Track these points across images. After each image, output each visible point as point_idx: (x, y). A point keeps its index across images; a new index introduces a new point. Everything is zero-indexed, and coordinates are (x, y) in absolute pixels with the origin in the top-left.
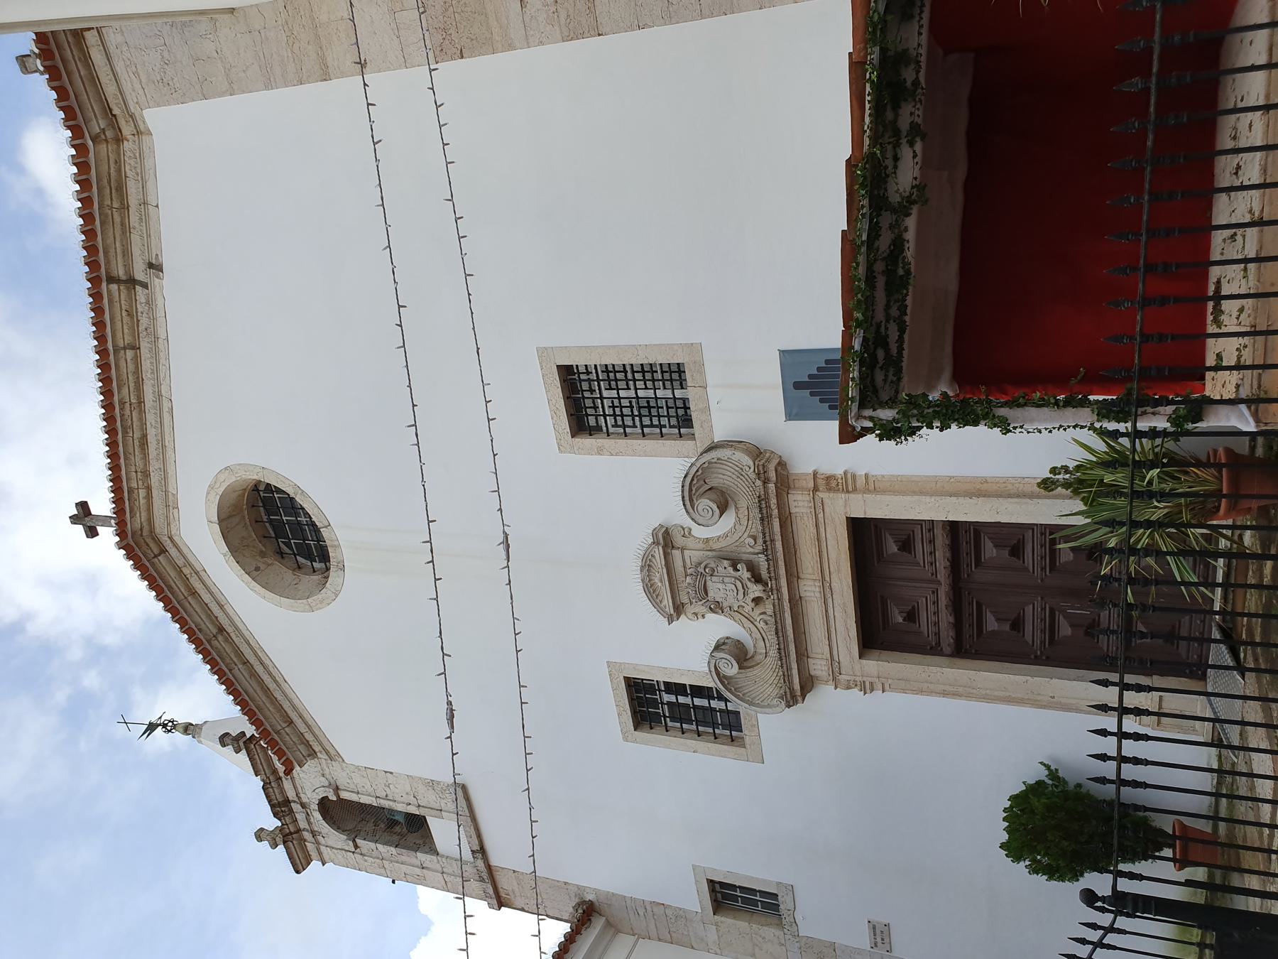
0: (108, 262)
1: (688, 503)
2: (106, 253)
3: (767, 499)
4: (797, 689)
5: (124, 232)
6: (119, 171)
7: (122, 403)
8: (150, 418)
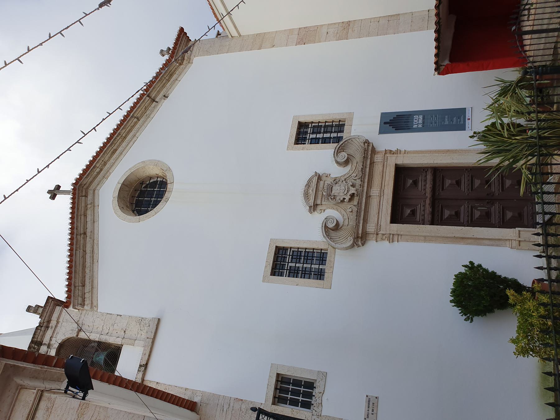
0: (151, 91)
1: (336, 154)
2: (153, 88)
3: (368, 151)
4: (360, 238)
5: (163, 86)
6: (175, 71)
7: (119, 134)
8: (124, 144)
